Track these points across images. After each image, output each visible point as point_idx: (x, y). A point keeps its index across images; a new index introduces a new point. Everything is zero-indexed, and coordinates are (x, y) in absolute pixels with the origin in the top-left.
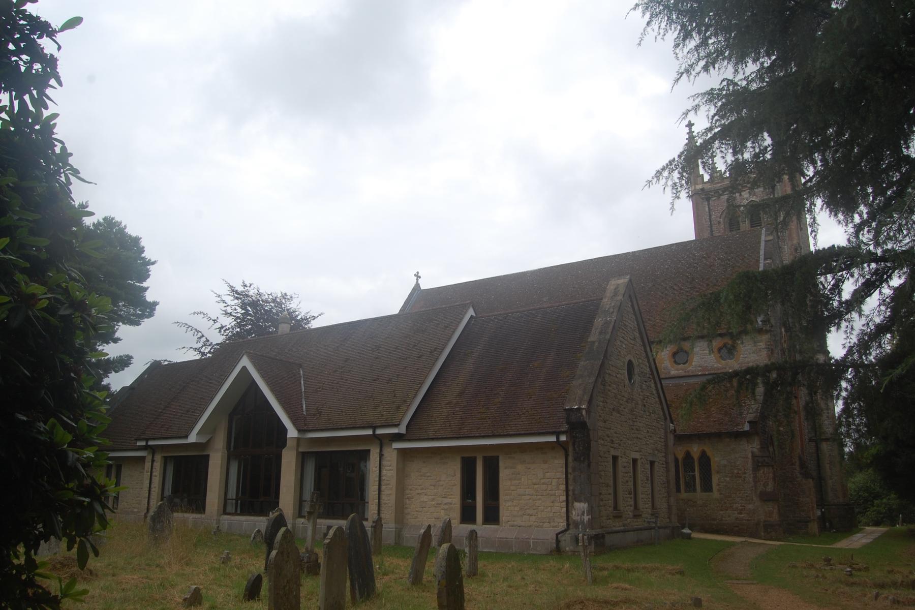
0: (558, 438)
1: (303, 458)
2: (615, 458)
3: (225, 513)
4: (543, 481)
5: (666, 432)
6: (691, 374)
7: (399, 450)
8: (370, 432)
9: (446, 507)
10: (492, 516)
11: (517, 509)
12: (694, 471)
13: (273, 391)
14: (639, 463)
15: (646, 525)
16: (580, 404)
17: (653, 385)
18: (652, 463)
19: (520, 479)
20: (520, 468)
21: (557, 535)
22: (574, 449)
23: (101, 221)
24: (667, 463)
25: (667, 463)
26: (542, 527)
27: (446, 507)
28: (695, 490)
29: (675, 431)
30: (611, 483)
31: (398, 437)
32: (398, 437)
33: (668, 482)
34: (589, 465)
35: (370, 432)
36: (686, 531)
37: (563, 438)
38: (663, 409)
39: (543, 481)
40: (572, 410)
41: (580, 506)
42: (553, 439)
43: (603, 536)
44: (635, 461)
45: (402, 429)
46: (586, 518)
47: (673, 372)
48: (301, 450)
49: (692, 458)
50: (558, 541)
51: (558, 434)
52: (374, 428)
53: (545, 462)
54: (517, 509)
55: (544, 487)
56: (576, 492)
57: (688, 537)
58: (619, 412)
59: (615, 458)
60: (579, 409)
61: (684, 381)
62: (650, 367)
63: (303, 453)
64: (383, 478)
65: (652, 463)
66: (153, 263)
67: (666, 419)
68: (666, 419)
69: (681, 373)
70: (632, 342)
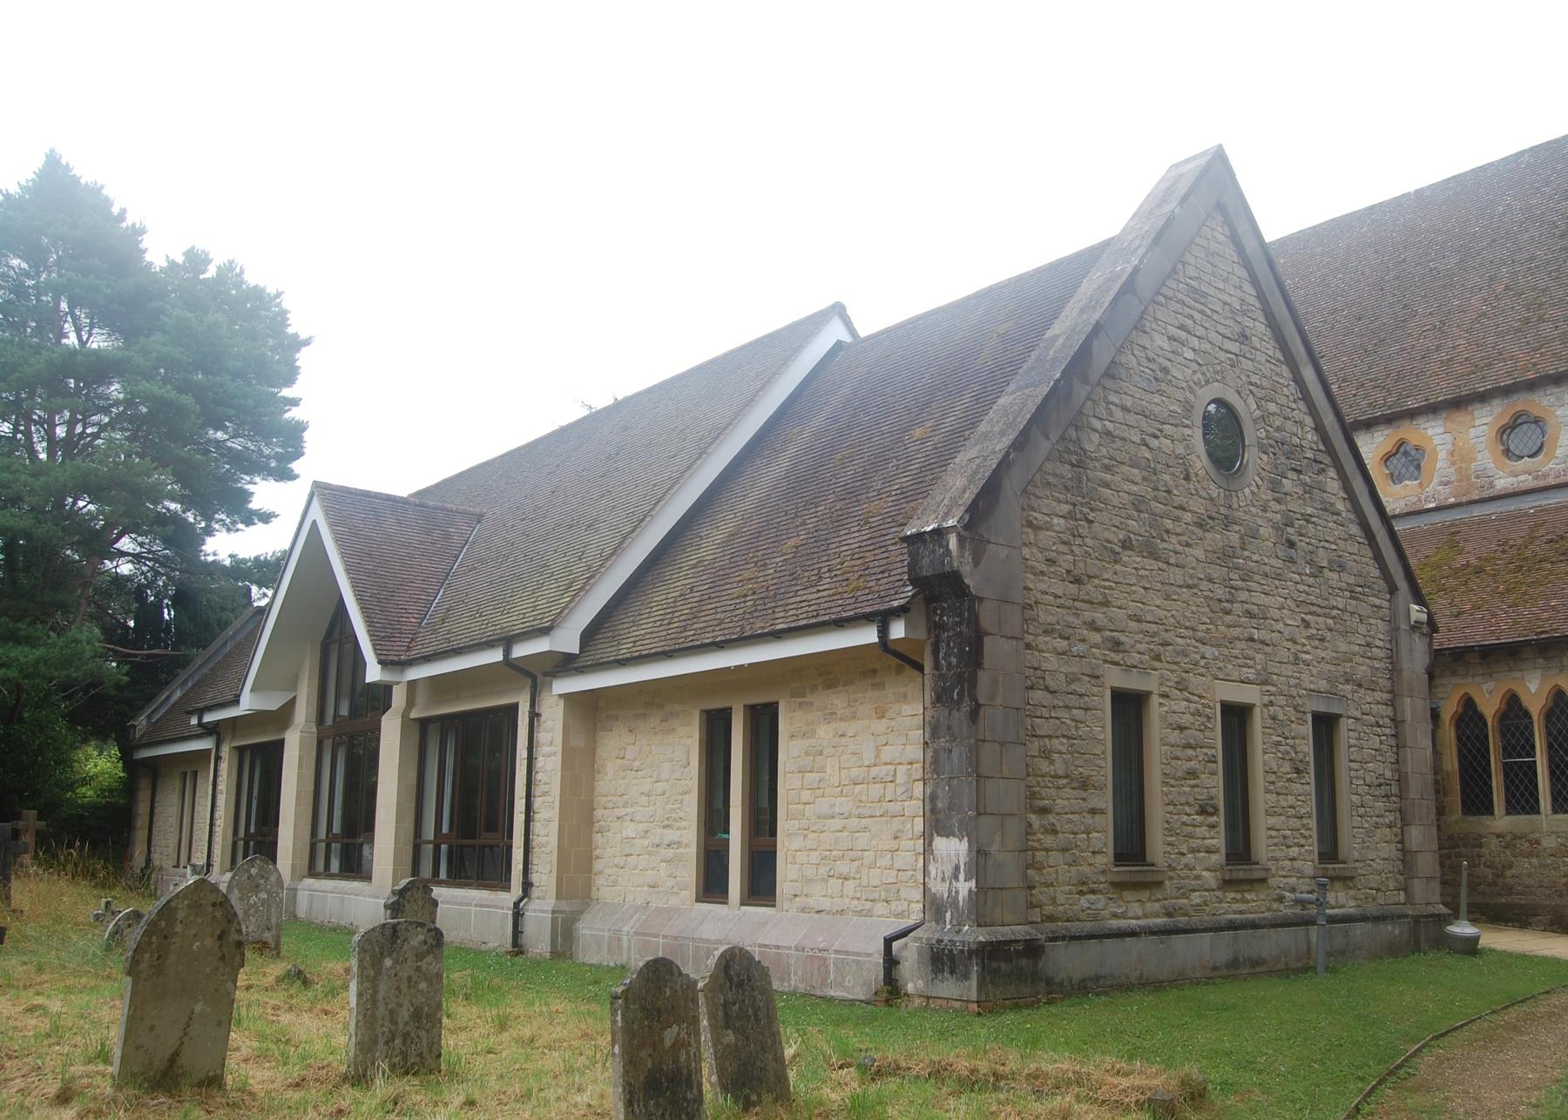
0: (883, 632)
1: (422, 731)
2: (1129, 706)
3: (312, 873)
4: (874, 771)
5: (1394, 630)
6: (1551, 481)
7: (568, 697)
8: (496, 656)
9: (670, 853)
10: (761, 887)
11: (814, 857)
12: (1531, 751)
13: (348, 570)
14: (1258, 720)
15: (1286, 910)
16: (946, 517)
17: (1333, 485)
18: (1325, 725)
19: (822, 770)
20: (824, 732)
21: (888, 942)
22: (937, 666)
23: (180, 259)
24: (1396, 721)
25: (1396, 721)
26: (869, 914)
27: (670, 853)
28: (1534, 808)
29: (1432, 625)
30: (1104, 770)
31: (565, 664)
32: (565, 664)
33: (1401, 780)
34: (974, 715)
35: (496, 656)
36: (1462, 928)
37: (898, 631)
38: (1378, 557)
39: (874, 771)
40: (919, 537)
41: (953, 849)
42: (868, 636)
43: (1032, 949)
44: (1236, 717)
45: (567, 640)
46: (964, 887)
47: (1503, 483)
48: (414, 715)
49: (1527, 714)
50: (891, 962)
51: (882, 619)
52: (508, 642)
53: (881, 714)
54: (814, 857)
55: (876, 790)
56: (940, 805)
57: (1470, 947)
58: (1154, 555)
59: (1129, 706)
60: (939, 533)
61: (1528, 504)
62: (1319, 428)
63: (424, 723)
64: (539, 776)
65: (1325, 725)
66: (307, 342)
67: (1393, 589)
68: (1393, 589)
69: (1527, 481)
70: (1234, 347)
